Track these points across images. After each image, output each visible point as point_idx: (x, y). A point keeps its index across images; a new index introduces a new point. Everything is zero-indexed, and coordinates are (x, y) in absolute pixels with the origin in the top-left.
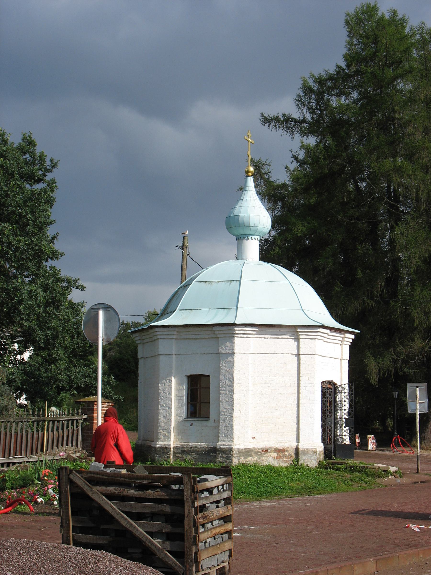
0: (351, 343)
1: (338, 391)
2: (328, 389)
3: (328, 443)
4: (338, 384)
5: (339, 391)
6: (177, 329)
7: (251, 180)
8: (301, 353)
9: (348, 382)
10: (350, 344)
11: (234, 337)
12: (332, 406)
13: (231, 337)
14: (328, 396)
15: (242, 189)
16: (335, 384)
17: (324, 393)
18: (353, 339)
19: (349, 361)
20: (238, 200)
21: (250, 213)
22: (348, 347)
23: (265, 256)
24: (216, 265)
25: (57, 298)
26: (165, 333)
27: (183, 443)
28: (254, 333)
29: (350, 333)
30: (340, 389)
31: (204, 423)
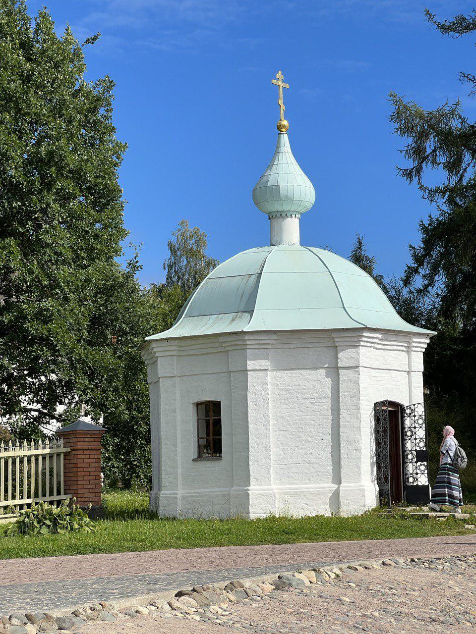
0: (425, 348)
1: (406, 415)
2: (382, 412)
3: (384, 484)
4: (406, 403)
5: (422, 418)
6: (176, 343)
7: (285, 139)
8: (340, 365)
9: (423, 402)
10: (424, 350)
11: (359, 346)
12: (387, 435)
13: (243, 348)
14: (382, 421)
15: (276, 150)
16: (401, 406)
17: (378, 417)
18: (428, 344)
19: (425, 374)
20: (270, 166)
21: (281, 183)
22: (421, 356)
23: (306, 240)
24: (238, 254)
25: (450, 212)
26: (166, 349)
27: (192, 491)
28: (273, 342)
29: (420, 334)
30: (408, 411)
31: (218, 462)
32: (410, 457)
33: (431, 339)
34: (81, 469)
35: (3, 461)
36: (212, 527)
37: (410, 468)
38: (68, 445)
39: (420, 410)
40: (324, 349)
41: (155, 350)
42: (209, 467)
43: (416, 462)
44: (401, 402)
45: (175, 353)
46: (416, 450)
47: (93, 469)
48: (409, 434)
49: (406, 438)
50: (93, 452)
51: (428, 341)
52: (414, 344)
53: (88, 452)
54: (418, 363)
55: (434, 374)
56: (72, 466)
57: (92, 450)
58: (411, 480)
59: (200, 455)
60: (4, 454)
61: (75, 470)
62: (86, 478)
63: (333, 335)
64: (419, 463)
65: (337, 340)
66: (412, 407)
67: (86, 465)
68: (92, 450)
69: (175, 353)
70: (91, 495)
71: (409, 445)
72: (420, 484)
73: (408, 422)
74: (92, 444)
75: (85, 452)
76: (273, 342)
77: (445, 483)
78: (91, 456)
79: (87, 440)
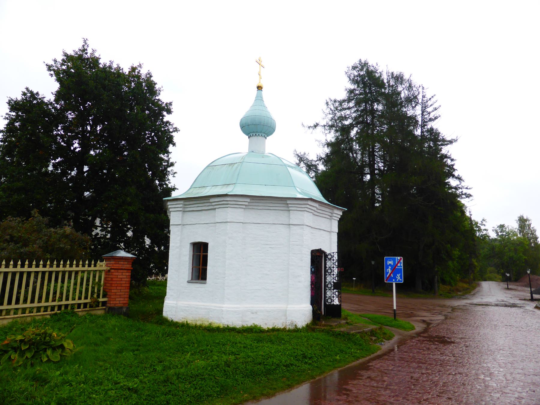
6: (182, 202)
16: (325, 253)
30: (329, 257)
32: (329, 286)
33: (343, 213)
34: (115, 282)
35: (2, 275)
36: (194, 333)
37: (329, 294)
38: (109, 265)
39: (336, 257)
40: (281, 212)
41: (169, 207)
42: (198, 287)
43: (333, 290)
44: (326, 251)
45: (181, 209)
46: (333, 282)
47: (124, 282)
48: (329, 271)
49: (327, 274)
50: (126, 271)
51: (341, 214)
52: (334, 215)
53: (122, 271)
54: (335, 228)
55: (343, 236)
56: (110, 279)
57: (124, 269)
58: (329, 301)
59: (192, 279)
60: (3, 269)
61: (111, 282)
62: (118, 288)
63: (288, 202)
64: (335, 291)
65: (290, 205)
66: (332, 254)
67: (119, 279)
68: (124, 269)
69: (181, 209)
70: (122, 299)
71: (329, 279)
72: (335, 303)
73: (329, 264)
74: (125, 266)
75: (119, 271)
76: (247, 204)
77: (200, 255)
78: (124, 274)
79: (122, 263)
